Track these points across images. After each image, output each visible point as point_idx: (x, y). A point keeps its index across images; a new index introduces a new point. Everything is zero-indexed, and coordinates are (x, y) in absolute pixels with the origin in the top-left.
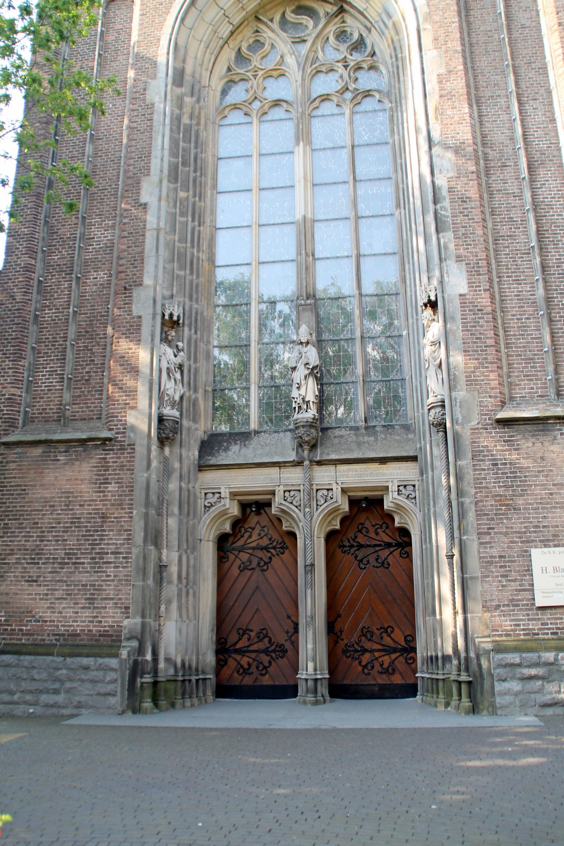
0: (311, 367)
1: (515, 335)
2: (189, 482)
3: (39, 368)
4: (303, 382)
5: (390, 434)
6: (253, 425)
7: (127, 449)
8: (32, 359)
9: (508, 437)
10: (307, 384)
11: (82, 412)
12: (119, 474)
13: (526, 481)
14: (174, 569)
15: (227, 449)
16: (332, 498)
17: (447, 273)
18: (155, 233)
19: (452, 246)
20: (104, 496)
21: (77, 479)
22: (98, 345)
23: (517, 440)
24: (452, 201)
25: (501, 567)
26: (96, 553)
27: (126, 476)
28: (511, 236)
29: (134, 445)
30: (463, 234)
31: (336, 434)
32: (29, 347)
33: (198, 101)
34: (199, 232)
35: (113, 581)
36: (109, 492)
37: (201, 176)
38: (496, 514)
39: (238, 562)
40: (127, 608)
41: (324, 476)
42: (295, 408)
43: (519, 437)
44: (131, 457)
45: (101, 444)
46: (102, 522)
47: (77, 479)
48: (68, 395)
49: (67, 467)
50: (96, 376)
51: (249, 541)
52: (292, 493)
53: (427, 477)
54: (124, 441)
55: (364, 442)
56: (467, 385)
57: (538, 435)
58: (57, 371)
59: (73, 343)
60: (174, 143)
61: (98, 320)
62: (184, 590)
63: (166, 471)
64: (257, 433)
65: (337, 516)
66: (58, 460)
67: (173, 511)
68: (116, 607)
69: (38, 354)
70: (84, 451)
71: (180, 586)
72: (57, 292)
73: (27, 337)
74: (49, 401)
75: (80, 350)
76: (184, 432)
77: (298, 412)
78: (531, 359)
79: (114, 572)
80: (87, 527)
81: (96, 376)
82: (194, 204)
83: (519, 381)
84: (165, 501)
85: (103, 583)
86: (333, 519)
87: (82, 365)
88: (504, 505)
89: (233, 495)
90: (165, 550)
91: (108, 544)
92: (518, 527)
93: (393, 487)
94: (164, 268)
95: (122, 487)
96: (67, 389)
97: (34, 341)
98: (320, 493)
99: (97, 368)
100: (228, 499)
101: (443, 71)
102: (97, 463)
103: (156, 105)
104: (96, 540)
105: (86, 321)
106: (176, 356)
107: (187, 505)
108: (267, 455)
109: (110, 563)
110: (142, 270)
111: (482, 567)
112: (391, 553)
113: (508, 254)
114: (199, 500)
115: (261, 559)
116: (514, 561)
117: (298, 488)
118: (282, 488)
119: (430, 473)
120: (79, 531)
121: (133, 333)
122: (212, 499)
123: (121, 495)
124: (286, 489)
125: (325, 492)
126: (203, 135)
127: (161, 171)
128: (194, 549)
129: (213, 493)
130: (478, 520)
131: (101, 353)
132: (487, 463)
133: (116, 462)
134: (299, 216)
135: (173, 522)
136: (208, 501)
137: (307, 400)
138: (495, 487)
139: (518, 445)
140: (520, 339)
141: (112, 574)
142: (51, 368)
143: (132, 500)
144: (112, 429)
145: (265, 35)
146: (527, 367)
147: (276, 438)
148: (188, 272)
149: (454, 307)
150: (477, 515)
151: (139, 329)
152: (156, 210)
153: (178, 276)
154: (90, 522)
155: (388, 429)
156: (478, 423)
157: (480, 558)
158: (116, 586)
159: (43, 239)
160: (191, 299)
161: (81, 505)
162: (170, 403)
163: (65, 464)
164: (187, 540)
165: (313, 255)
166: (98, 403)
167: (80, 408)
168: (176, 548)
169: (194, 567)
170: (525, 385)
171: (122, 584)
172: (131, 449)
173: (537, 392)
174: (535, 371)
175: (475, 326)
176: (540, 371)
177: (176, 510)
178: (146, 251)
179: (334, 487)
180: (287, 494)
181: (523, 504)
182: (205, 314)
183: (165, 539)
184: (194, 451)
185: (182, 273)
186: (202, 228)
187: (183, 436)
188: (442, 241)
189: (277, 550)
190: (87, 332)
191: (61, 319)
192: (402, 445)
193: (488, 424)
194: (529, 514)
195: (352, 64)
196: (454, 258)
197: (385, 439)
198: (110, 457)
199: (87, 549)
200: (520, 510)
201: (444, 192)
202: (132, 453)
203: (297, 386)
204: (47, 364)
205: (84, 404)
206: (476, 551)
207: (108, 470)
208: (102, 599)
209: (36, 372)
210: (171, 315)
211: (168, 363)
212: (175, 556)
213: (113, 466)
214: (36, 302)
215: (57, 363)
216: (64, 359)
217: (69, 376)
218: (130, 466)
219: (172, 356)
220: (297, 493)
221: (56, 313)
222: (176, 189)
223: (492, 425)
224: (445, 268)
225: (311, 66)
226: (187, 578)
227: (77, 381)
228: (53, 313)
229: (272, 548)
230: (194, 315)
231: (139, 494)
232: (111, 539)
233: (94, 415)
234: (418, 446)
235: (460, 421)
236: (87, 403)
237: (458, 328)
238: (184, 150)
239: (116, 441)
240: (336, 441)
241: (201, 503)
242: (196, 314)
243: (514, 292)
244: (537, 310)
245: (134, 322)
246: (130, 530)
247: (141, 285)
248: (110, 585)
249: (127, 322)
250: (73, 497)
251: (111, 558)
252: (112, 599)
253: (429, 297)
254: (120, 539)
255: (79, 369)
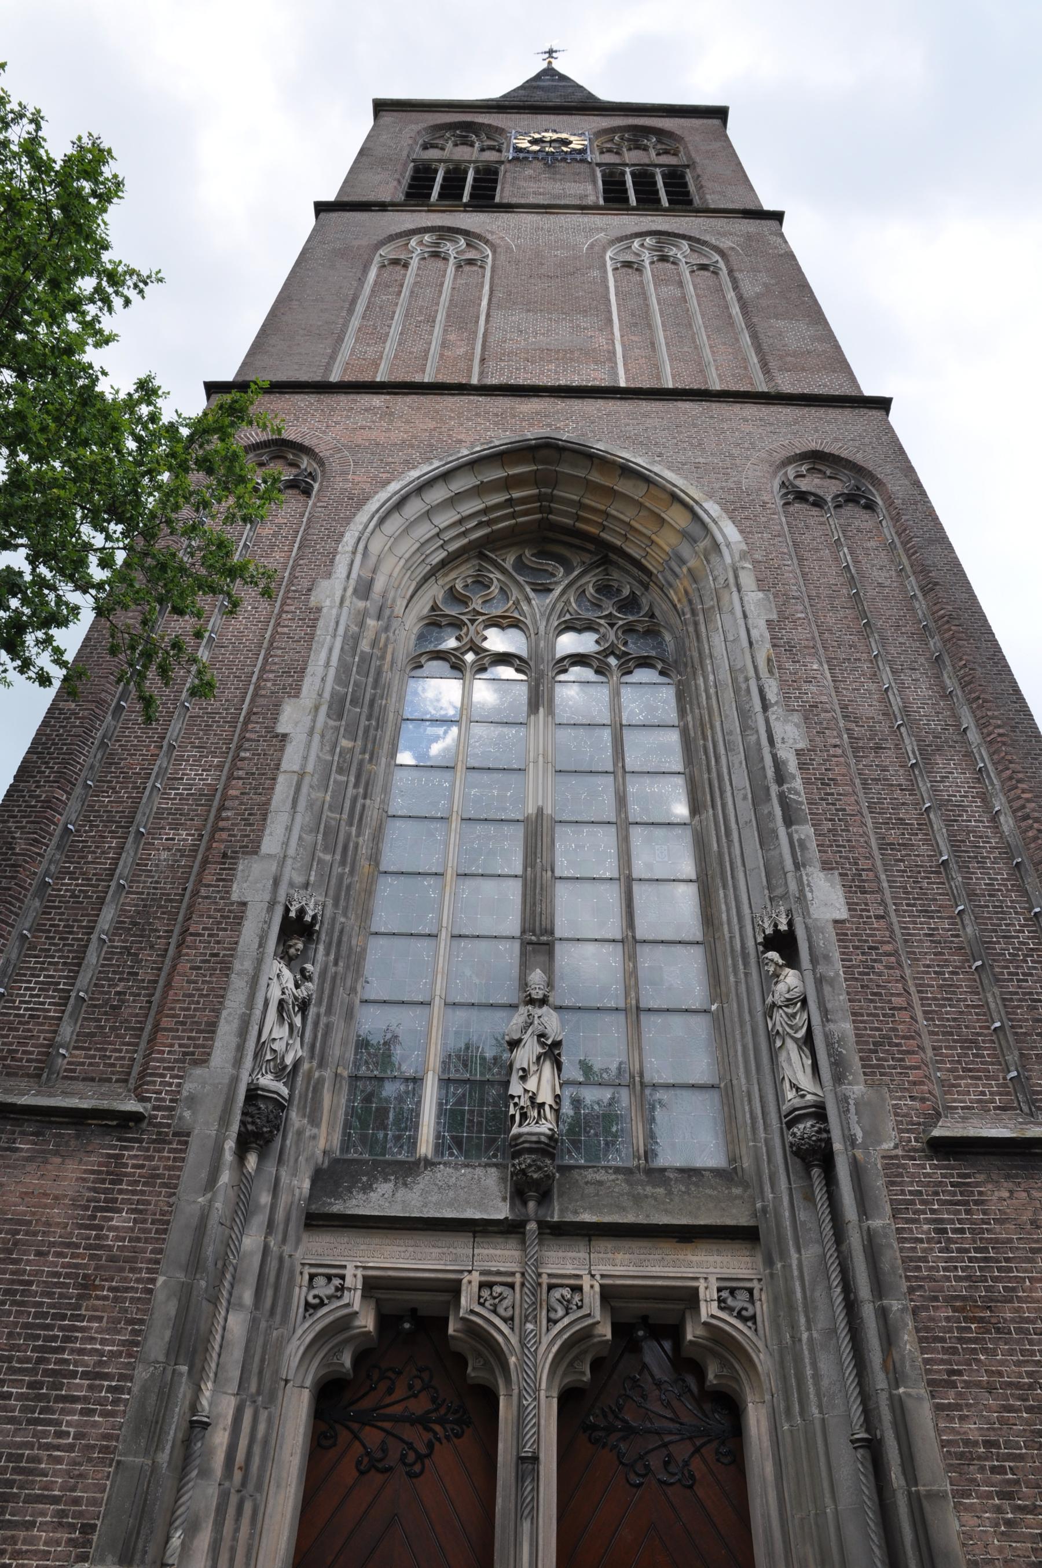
0: (549, 1042)
1: (935, 999)
2: (284, 1241)
3: (25, 975)
4: (533, 1068)
5: (696, 1185)
6: (425, 1147)
7: (170, 1143)
8: (14, 956)
9: (959, 1176)
10: (539, 1071)
11: (90, 1064)
12: (142, 1193)
13: (1010, 1270)
14: (220, 1438)
15: (367, 1188)
16: (579, 1308)
17: (809, 885)
18: (295, 777)
19: (812, 845)
20: (98, 1237)
21: (46, 1195)
22: (152, 947)
23: (977, 1184)
24: (807, 782)
25: (994, 1470)
26: (47, 1373)
27: (157, 1201)
28: (904, 845)
29: (188, 1135)
30: (830, 830)
31: (589, 1177)
32: (15, 933)
33: (387, 629)
34: (364, 806)
35: (71, 1448)
36: (111, 1229)
37: (377, 729)
38: (960, 1340)
39: (357, 1449)
40: (88, 1529)
41: (563, 1261)
42: (513, 1116)
43: (981, 1178)
44: (175, 1159)
45: (117, 1126)
46: (80, 1297)
47: (46, 1195)
48: (69, 1030)
49: (31, 1167)
50: (134, 1001)
51: (388, 1400)
52: (498, 1289)
53: (787, 1267)
54: (169, 1126)
55: (646, 1196)
56: (865, 1074)
57: (1017, 1176)
58: (59, 983)
59: (104, 937)
60: (344, 668)
61: (160, 907)
62: (234, 1499)
63: (243, 1207)
64: (429, 1163)
65: (585, 1352)
66: (17, 1150)
67: (240, 1298)
68: (60, 1524)
69: (28, 949)
70: (77, 1137)
71: (227, 1484)
72: (94, 852)
73: (17, 915)
74: (26, 1038)
75: (112, 953)
76: (290, 1136)
77: (520, 1125)
78: (971, 1041)
79: (78, 1424)
80: (40, 1304)
81: (134, 1001)
82: (361, 763)
83: (957, 1078)
84: (231, 1268)
85: (44, 1454)
86: (576, 1358)
87: (113, 980)
88: (973, 1320)
89: (372, 1286)
90: (210, 1385)
91: (81, 1352)
92: (1010, 1373)
93: (708, 1292)
94: (300, 838)
95: (144, 1221)
96: (70, 1017)
97: (27, 925)
98: (557, 1294)
99: (139, 988)
100: (359, 1293)
101: (775, 617)
102: (100, 1164)
103: (325, 610)
104: (54, 1338)
105: (136, 905)
106: (297, 986)
107: (272, 1283)
108: (450, 1205)
109: (75, 1400)
110: (263, 831)
111: (950, 1468)
112: (697, 1450)
113: (905, 871)
114: (297, 1289)
115: (410, 1446)
116: (1021, 1458)
117: (509, 1280)
118: (476, 1277)
119: (794, 1256)
120: (19, 1314)
121: (226, 930)
122: (323, 1289)
123: (138, 1240)
124: (484, 1278)
125: (566, 1293)
126: (387, 675)
127: (320, 695)
128: (272, 1398)
129: (329, 1278)
130: (923, 1351)
131: (155, 962)
132: (926, 1227)
133: (142, 1166)
134: (531, 810)
135: (237, 1324)
136: (315, 1292)
137: (539, 1100)
138: (948, 1279)
139: (980, 1193)
140: (945, 1006)
141: (72, 1430)
142: (45, 976)
143: (160, 1251)
144: (149, 1100)
145: (491, 576)
146: (966, 1055)
147: (469, 1176)
148: (338, 857)
149: (828, 941)
150: (921, 1340)
151: (239, 924)
152: (302, 746)
153: (320, 861)
154: (50, 1295)
155: (690, 1177)
156: (896, 1147)
157: (944, 1444)
158: (74, 1463)
159: (92, 767)
160: (336, 905)
161: (39, 1254)
162: (275, 1067)
163: (29, 1159)
164: (261, 1373)
165: (553, 871)
166: (127, 1051)
167: (86, 1057)
168: (233, 1387)
169: (266, 1442)
170: (967, 1085)
171: (90, 1460)
172: (180, 1143)
173: (993, 1101)
174: (982, 1063)
175: (868, 974)
176: (992, 1064)
177: (248, 1297)
178: (274, 803)
179: (586, 1282)
180: (486, 1293)
181: (1013, 1320)
182: (354, 942)
183: (215, 1355)
184: (302, 1181)
185: (328, 857)
186: (368, 801)
187: (288, 1142)
188: (796, 837)
189: (448, 1426)
190: (135, 924)
191: (91, 897)
192: (723, 1205)
193: (915, 1150)
194: (1031, 1343)
195: (621, 623)
196: (818, 865)
197: (687, 1192)
198: (132, 1156)
199: (28, 1360)
200: (1010, 1333)
201: (792, 766)
202: (181, 1151)
203: (521, 1073)
204: (42, 969)
205: (97, 1049)
206: (931, 1425)
207: (121, 1182)
208: (31, 1499)
209: (15, 981)
210: (302, 912)
211: (283, 993)
212: (228, 1405)
213: (133, 1174)
214: (50, 862)
215: (63, 971)
216: (79, 965)
217: (81, 994)
218: (170, 1177)
219: (291, 985)
220: (506, 1291)
221: (82, 885)
222: (337, 729)
223: (923, 1151)
224: (805, 878)
225: (559, 617)
226: (246, 1468)
227: (95, 1006)
228: (77, 885)
229: (435, 1422)
230: (336, 934)
231: (178, 1241)
232: (92, 1340)
233: (113, 1073)
234: (759, 1205)
235: (860, 1141)
236: (106, 1050)
237: (838, 975)
238: (356, 684)
239: (150, 1124)
240: (590, 1190)
241: (300, 1294)
242: (341, 932)
243: (922, 929)
244: (968, 961)
245: (230, 911)
246: (141, 1322)
247: (256, 853)
248: (58, 1460)
249: (219, 911)
250: (27, 1233)
251: (79, 1387)
252: (56, 1500)
253: (776, 925)
254: (112, 1343)
255: (103, 986)
